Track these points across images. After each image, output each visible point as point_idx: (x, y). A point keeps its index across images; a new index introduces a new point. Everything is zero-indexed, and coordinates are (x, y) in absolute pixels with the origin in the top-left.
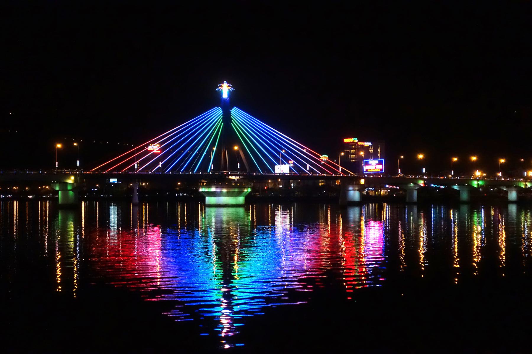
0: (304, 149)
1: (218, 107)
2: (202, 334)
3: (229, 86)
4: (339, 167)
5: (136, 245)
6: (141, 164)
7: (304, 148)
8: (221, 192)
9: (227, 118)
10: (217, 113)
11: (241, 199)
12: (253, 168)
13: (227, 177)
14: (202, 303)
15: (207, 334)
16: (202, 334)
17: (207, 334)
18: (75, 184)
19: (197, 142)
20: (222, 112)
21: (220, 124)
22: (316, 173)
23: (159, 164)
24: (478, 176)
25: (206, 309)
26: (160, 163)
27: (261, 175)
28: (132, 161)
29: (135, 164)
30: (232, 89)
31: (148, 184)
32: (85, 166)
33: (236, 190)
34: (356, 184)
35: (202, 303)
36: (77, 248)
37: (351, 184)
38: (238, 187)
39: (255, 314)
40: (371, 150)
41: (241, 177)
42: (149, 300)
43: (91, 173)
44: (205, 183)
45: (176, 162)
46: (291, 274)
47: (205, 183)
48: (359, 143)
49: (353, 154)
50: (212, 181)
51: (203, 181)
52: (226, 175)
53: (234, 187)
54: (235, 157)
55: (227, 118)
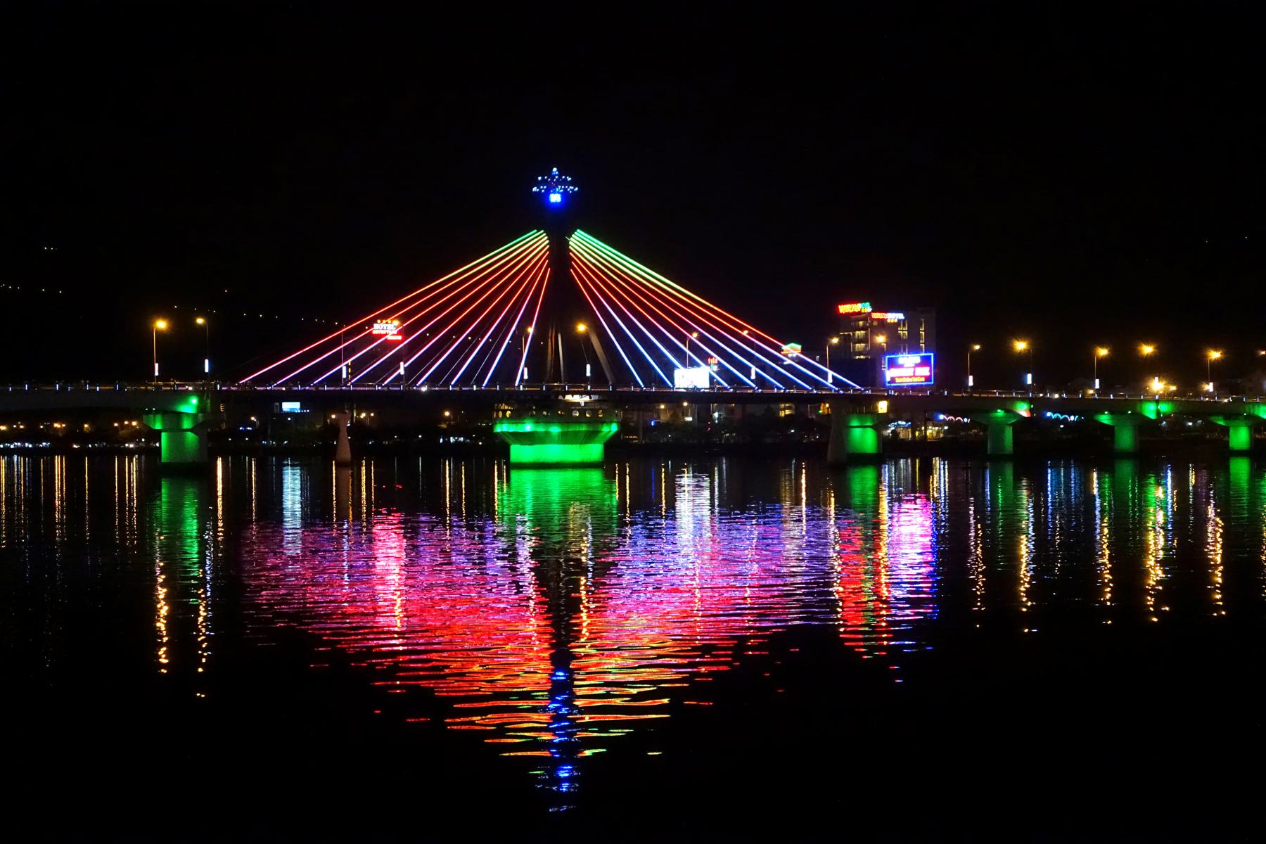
8: (547, 433)
11: (594, 451)
13: (561, 397)
18: (200, 415)
20: (548, 241)
26: (402, 364)
28: (336, 360)
31: (372, 415)
32: (226, 371)
33: (584, 428)
34: (867, 413)
38: (588, 422)
40: (903, 332)
41: (594, 397)
44: (508, 413)
48: (876, 315)
49: (860, 341)
50: (524, 406)
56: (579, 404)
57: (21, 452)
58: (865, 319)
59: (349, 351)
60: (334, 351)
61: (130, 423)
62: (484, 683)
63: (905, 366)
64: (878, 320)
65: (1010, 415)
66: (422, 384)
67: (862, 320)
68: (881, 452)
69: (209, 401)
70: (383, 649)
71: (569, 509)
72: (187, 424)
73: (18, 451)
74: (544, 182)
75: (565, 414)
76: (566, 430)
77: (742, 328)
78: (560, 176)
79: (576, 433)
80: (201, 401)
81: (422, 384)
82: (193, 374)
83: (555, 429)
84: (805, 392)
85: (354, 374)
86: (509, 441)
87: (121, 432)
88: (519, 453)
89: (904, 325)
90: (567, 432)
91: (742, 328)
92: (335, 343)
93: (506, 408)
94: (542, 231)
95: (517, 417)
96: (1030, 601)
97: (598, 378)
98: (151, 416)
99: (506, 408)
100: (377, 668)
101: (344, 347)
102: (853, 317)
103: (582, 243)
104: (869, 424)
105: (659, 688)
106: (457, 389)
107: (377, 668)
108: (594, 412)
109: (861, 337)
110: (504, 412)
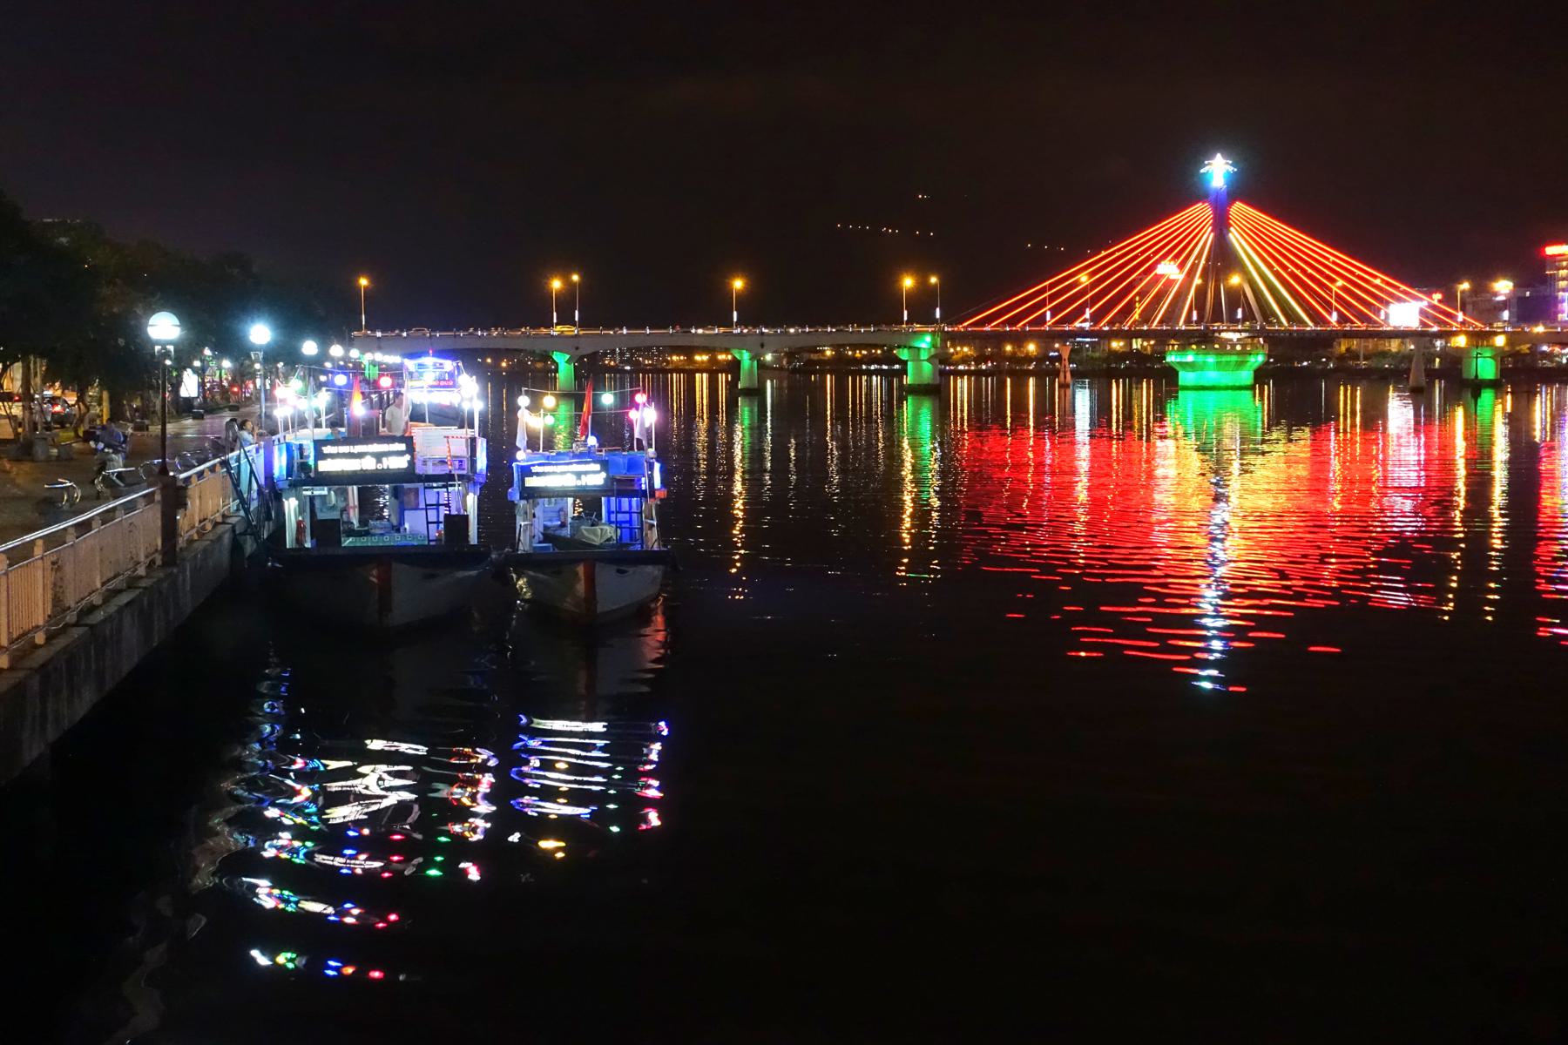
0: (1201, 276)
1: (1204, 203)
3: (1227, 163)
5: (1339, 472)
7: (1375, 277)
10: (1201, 212)
11: (1246, 376)
12: (1267, 314)
14: (1351, 584)
19: (1128, 270)
22: (1301, 322)
23: (1091, 314)
25: (1549, 620)
26: (1087, 310)
28: (1042, 304)
29: (1045, 312)
30: (1232, 168)
33: (1234, 358)
34: (1487, 346)
35: (1351, 584)
36: (828, 438)
37: (141, 317)
38: (1239, 353)
44: (1176, 347)
45: (1074, 306)
46: (1327, 527)
47: (1176, 347)
49: (1563, 279)
50: (1187, 340)
51: (1173, 342)
52: (1214, 331)
54: (1236, 298)
59: (1053, 297)
60: (1119, 288)
61: (962, 348)
66: (1104, 326)
67: (1565, 261)
68: (1499, 377)
69: (939, 339)
70: (1398, 578)
71: (147, 419)
72: (924, 355)
73: (877, 372)
75: (1224, 348)
76: (1220, 360)
77: (1375, 277)
79: (1228, 363)
80: (933, 339)
81: (1104, 326)
82: (928, 320)
83: (1211, 359)
85: (1339, 288)
86: (1178, 368)
88: (1185, 378)
90: (1221, 362)
91: (1375, 277)
92: (1043, 291)
94: (1206, 204)
95: (1184, 348)
97: (1249, 315)
98: (901, 350)
100: (1558, 621)
101: (1050, 296)
104: (1489, 355)
107: (1558, 621)
108: (1244, 346)
110: (1173, 345)
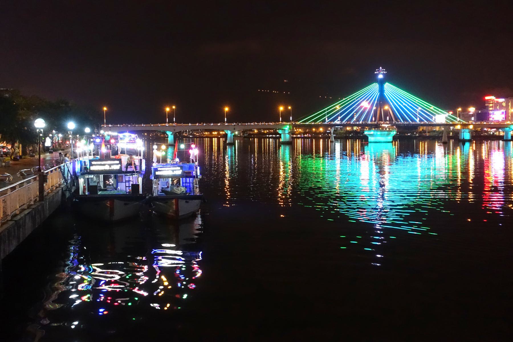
2: (420, 234)
4: (432, 117)
6: (328, 118)
7: (431, 107)
9: (382, 90)
11: (390, 138)
12: (397, 119)
15: (342, 237)
16: (420, 234)
17: (342, 237)
18: (289, 130)
20: (378, 87)
21: (377, 94)
24: (80, 140)
27: (410, 124)
28: (325, 115)
32: (296, 119)
33: (386, 133)
34: (467, 128)
38: (388, 131)
39: (409, 222)
40: (504, 104)
42: (320, 207)
43: (299, 124)
49: (491, 107)
51: (367, 127)
53: (386, 131)
54: (387, 113)
55: (382, 90)
56: (385, 127)
57: (272, 138)
58: (492, 101)
59: (328, 113)
62: (175, 148)
63: (125, 144)
64: (497, 101)
65: (510, 129)
73: (271, 137)
74: (378, 71)
78: (382, 69)
83: (379, 133)
84: (449, 123)
86: (368, 136)
87: (297, 132)
88: (370, 139)
89: (504, 102)
91: (431, 107)
92: (325, 111)
93: (367, 128)
96: (52, 131)
99: (367, 128)
102: (489, 100)
103: (388, 87)
105: (432, 204)
106: (354, 123)
108: (389, 129)
109: (491, 106)
